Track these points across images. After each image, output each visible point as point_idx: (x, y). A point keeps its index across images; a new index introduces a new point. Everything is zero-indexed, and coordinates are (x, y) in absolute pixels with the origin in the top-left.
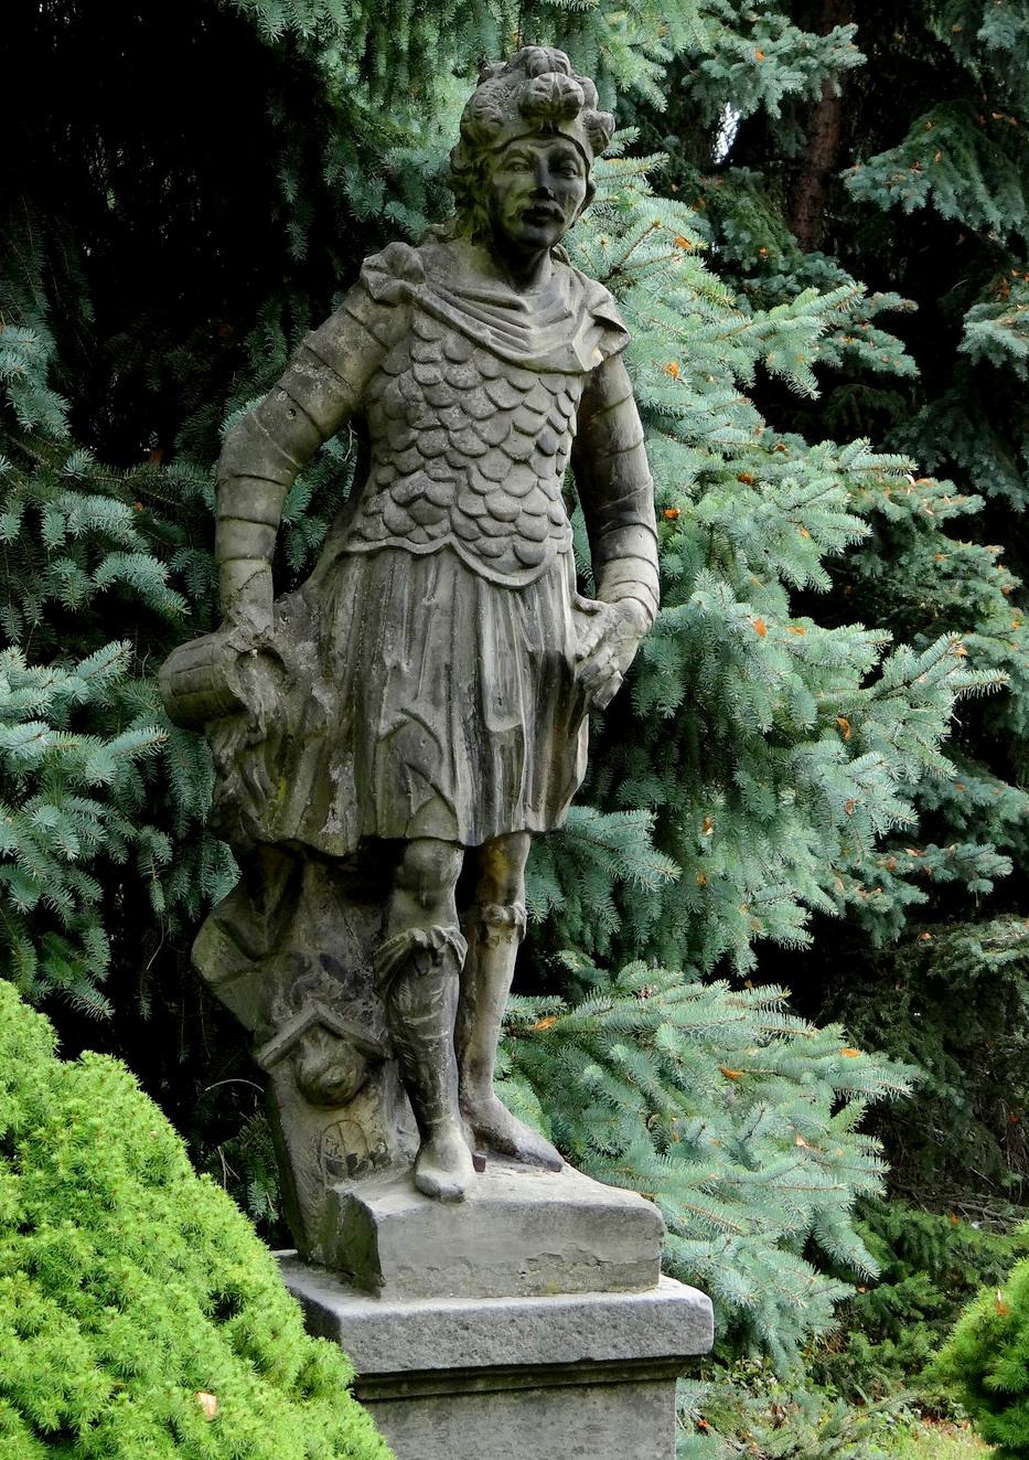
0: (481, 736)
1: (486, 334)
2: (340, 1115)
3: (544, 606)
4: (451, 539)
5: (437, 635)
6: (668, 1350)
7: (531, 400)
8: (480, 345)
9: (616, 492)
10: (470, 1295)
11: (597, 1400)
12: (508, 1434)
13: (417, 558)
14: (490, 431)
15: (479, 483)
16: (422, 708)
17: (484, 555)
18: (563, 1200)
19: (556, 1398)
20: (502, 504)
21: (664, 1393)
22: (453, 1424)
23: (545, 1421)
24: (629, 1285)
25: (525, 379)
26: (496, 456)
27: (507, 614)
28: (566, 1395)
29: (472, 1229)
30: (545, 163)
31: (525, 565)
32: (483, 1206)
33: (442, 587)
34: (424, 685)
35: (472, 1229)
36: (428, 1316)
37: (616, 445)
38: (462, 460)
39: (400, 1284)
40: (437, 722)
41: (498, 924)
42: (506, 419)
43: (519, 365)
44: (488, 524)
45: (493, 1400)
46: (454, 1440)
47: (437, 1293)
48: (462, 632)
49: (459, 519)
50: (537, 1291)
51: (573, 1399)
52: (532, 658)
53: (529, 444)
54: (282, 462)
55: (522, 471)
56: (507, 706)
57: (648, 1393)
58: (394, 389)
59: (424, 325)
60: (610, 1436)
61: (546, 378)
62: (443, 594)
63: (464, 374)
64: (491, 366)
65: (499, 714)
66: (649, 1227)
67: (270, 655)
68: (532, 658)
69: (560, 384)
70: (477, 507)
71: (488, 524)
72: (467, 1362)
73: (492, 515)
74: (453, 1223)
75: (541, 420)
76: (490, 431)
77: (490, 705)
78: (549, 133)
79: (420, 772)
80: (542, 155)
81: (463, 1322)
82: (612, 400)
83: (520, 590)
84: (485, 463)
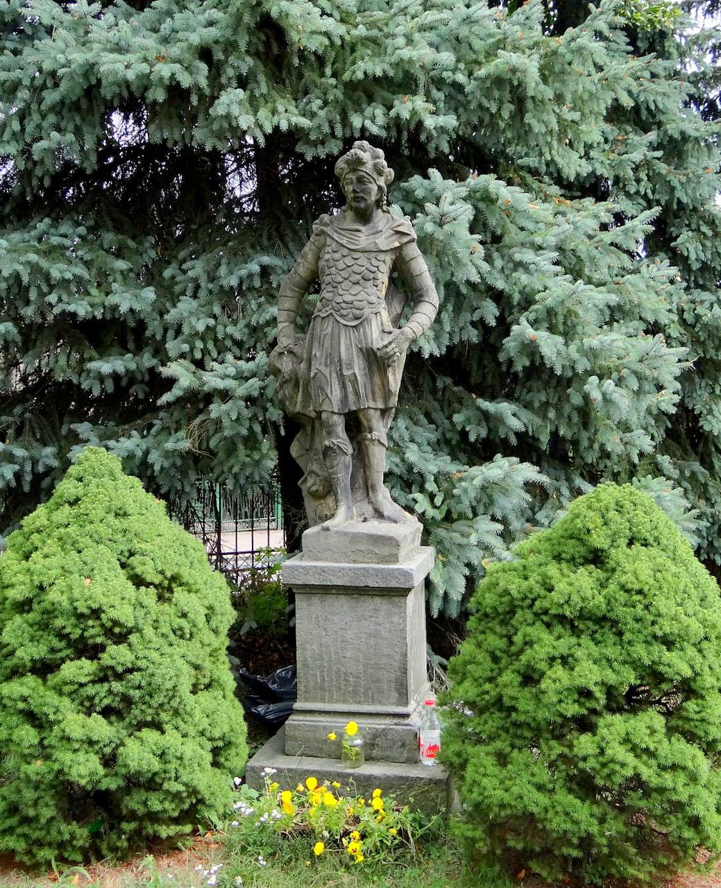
0: (341, 376)
1: (344, 242)
2: (322, 501)
3: (364, 331)
4: (332, 311)
5: (327, 344)
6: (397, 585)
7: (359, 262)
8: (342, 245)
9: (416, 291)
10: (331, 561)
11: (377, 600)
12: (345, 608)
13: (323, 318)
14: (344, 274)
15: (341, 292)
16: (322, 368)
17: (342, 316)
18: (364, 531)
19: (362, 598)
20: (348, 298)
21: (402, 600)
22: (326, 603)
23: (359, 605)
24: (387, 562)
25: (356, 255)
26: (347, 282)
27: (366, 339)
28: (366, 597)
29: (332, 540)
30: (355, 180)
31: (357, 318)
32: (337, 532)
33: (329, 328)
34: (323, 360)
35: (332, 540)
36: (311, 567)
37: (415, 274)
38: (335, 285)
39: (309, 556)
40: (326, 372)
41: (368, 439)
42: (350, 269)
43: (355, 251)
44: (343, 305)
45: (340, 597)
46: (327, 608)
47: (321, 560)
48: (335, 342)
49: (334, 304)
50: (355, 561)
51: (369, 599)
52: (361, 349)
53: (359, 277)
54: (293, 291)
55: (357, 286)
56: (350, 366)
57: (396, 599)
58: (322, 263)
59: (329, 240)
60: (382, 613)
61: (366, 254)
62: (329, 329)
63: (337, 256)
64: (345, 252)
65: (348, 369)
66: (394, 543)
67: (291, 352)
68: (361, 349)
69: (381, 257)
70: (339, 300)
71: (343, 305)
72: (325, 583)
73: (344, 302)
74: (326, 538)
75: (363, 269)
76: (344, 274)
77: (344, 366)
78: (354, 170)
79: (322, 389)
80: (354, 178)
81: (323, 570)
82: (407, 259)
83: (355, 327)
84: (343, 285)
